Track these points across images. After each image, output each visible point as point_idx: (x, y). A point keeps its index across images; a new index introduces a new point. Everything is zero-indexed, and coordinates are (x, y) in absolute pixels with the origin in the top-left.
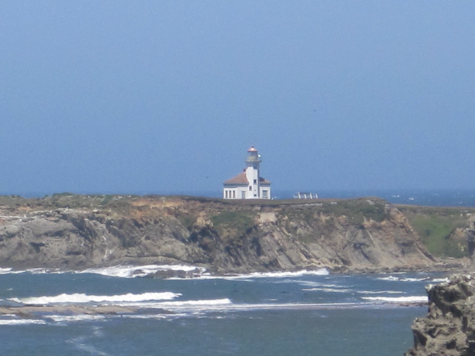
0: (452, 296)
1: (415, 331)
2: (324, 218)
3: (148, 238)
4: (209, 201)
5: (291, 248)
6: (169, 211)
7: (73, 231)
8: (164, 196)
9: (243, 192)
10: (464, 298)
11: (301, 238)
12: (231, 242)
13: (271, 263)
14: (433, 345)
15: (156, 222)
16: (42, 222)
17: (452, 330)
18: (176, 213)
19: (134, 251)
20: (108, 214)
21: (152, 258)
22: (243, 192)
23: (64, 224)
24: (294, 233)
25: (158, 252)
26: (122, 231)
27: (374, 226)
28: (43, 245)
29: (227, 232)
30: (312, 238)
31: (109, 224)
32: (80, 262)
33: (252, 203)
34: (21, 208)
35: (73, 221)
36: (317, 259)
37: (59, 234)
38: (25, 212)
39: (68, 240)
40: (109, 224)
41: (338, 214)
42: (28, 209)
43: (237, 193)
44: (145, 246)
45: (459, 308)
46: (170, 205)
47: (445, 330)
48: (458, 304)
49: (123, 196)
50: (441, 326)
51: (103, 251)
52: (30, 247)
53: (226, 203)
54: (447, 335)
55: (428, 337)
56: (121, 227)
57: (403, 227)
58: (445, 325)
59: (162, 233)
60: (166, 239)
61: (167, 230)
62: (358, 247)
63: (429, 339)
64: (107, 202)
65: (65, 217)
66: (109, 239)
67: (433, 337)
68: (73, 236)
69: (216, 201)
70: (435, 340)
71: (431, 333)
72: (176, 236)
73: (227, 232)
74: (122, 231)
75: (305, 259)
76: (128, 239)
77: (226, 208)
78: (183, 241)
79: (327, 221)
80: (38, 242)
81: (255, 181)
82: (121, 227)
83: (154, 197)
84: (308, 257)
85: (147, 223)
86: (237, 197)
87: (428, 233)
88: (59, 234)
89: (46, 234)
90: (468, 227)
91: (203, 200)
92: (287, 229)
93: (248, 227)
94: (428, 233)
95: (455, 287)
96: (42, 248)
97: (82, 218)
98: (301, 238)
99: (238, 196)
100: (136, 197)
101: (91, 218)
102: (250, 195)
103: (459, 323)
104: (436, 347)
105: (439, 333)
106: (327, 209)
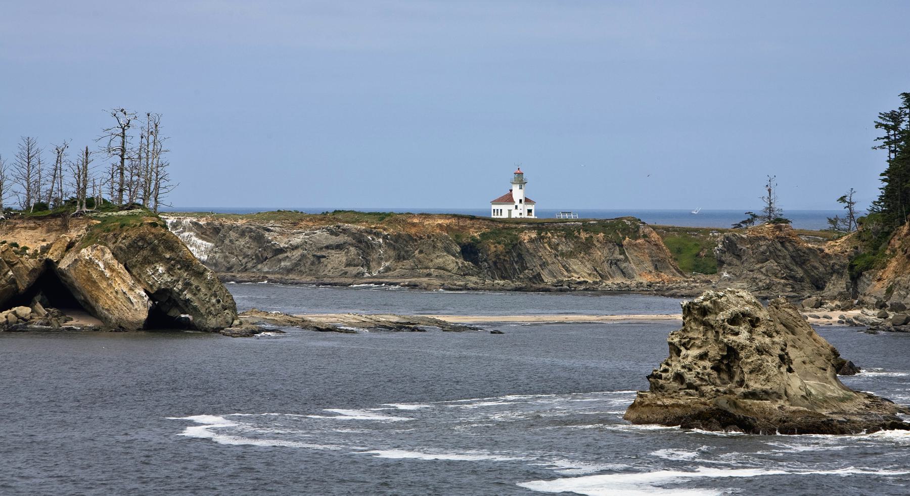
0: (704, 311)
1: (670, 344)
2: (584, 235)
3: (421, 252)
4: (479, 219)
5: (553, 263)
6: (440, 226)
7: (352, 245)
8: (121, 328)
9: (510, 211)
10: (716, 314)
11: (562, 254)
12: (497, 256)
13: (535, 277)
14: (687, 356)
15: (429, 237)
16: (322, 236)
17: (705, 342)
18: (448, 228)
19: (408, 263)
20: (385, 229)
21: (425, 271)
22: (510, 211)
23: (341, 239)
24: (556, 250)
25: (430, 264)
26: (397, 245)
27: (630, 244)
28: (324, 257)
29: (494, 248)
30: (571, 255)
31: (385, 238)
32: (358, 274)
33: (518, 221)
34: (304, 223)
35: (353, 235)
36: (577, 273)
37: (339, 247)
38: (307, 227)
39: (347, 253)
40: (385, 238)
41: (597, 233)
42: (311, 224)
43: (505, 211)
44: (418, 259)
45: (712, 323)
46: (440, 222)
47: (698, 342)
48: (710, 318)
49: (247, 218)
50: (694, 339)
51: (379, 264)
52: (312, 259)
53: (493, 220)
54: (700, 347)
55: (682, 348)
56: (396, 241)
57: (656, 245)
58: (698, 338)
59: (434, 247)
60: (438, 253)
61: (439, 245)
62: (615, 263)
63: (684, 352)
64: (381, 216)
65: (345, 231)
66: (385, 252)
67: (687, 349)
68: (352, 249)
69: (484, 219)
70: (689, 352)
71: (684, 345)
72: (448, 250)
73: (494, 248)
74: (397, 245)
75: (566, 273)
76: (403, 253)
77: (493, 225)
78: (454, 255)
79: (587, 239)
80: (319, 254)
81: (521, 201)
82: (396, 241)
83: (426, 215)
84: (568, 270)
85: (421, 238)
86: (513, 216)
87: (679, 251)
88: (339, 247)
89: (327, 247)
90: (717, 246)
91: (472, 218)
92: (550, 245)
93: (515, 242)
94: (679, 251)
95: (707, 303)
96: (322, 260)
97: (361, 231)
98: (562, 254)
99: (505, 215)
100: (409, 214)
101: (370, 233)
102: (515, 214)
103: (711, 335)
104: (690, 359)
105: (693, 345)
106: (586, 226)
